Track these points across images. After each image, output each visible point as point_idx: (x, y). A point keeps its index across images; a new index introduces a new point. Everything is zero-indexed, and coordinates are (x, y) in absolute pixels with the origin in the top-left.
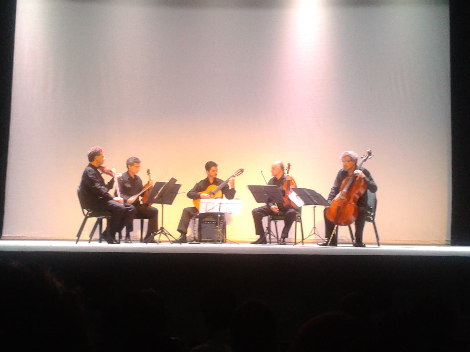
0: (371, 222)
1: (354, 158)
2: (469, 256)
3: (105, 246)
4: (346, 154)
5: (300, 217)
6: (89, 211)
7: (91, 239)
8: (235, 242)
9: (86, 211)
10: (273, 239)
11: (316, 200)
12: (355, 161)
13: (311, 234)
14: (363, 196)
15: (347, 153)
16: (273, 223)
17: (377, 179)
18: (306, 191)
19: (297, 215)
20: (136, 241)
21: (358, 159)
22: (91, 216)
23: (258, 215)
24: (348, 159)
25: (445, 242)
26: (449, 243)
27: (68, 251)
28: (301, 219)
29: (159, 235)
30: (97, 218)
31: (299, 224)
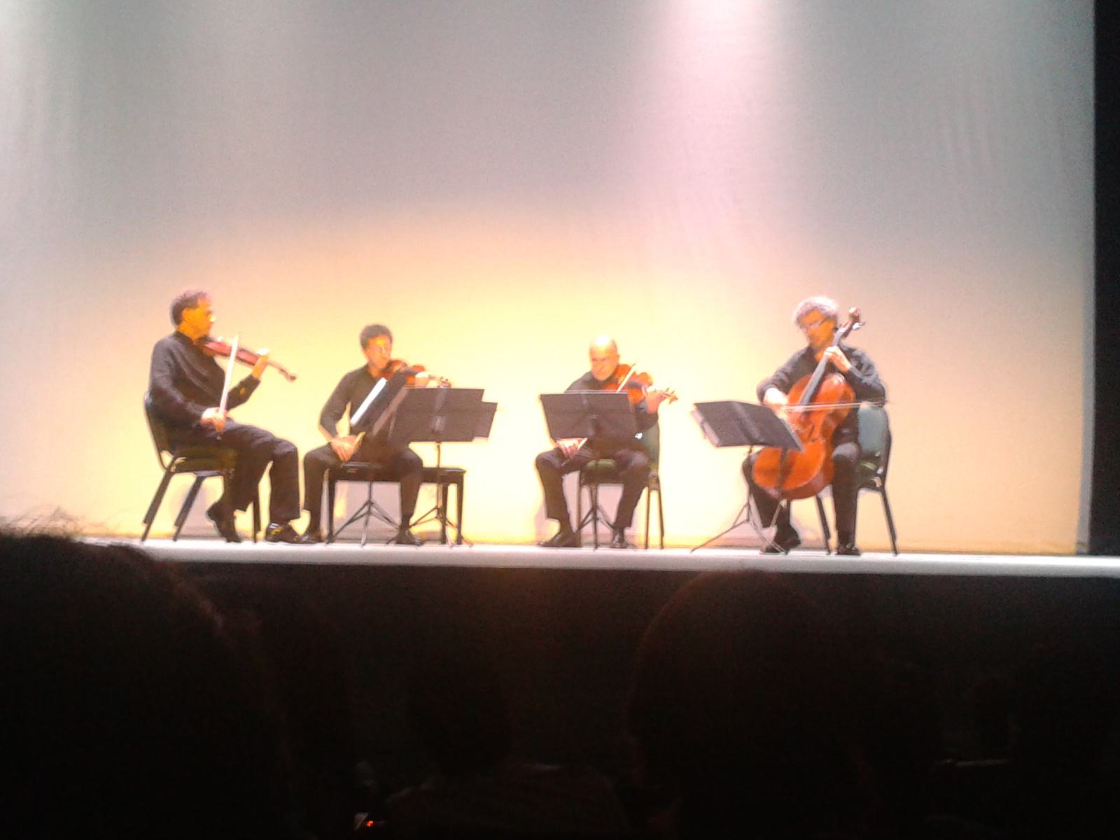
2: (1116, 576)
7: (179, 530)
9: (167, 458)
12: (831, 319)
13: (737, 523)
17: (886, 373)
18: (739, 409)
21: (839, 316)
22: (181, 469)
25: (1073, 548)
26: (1085, 550)
27: (633, 567)
28: (658, 481)
31: (654, 495)
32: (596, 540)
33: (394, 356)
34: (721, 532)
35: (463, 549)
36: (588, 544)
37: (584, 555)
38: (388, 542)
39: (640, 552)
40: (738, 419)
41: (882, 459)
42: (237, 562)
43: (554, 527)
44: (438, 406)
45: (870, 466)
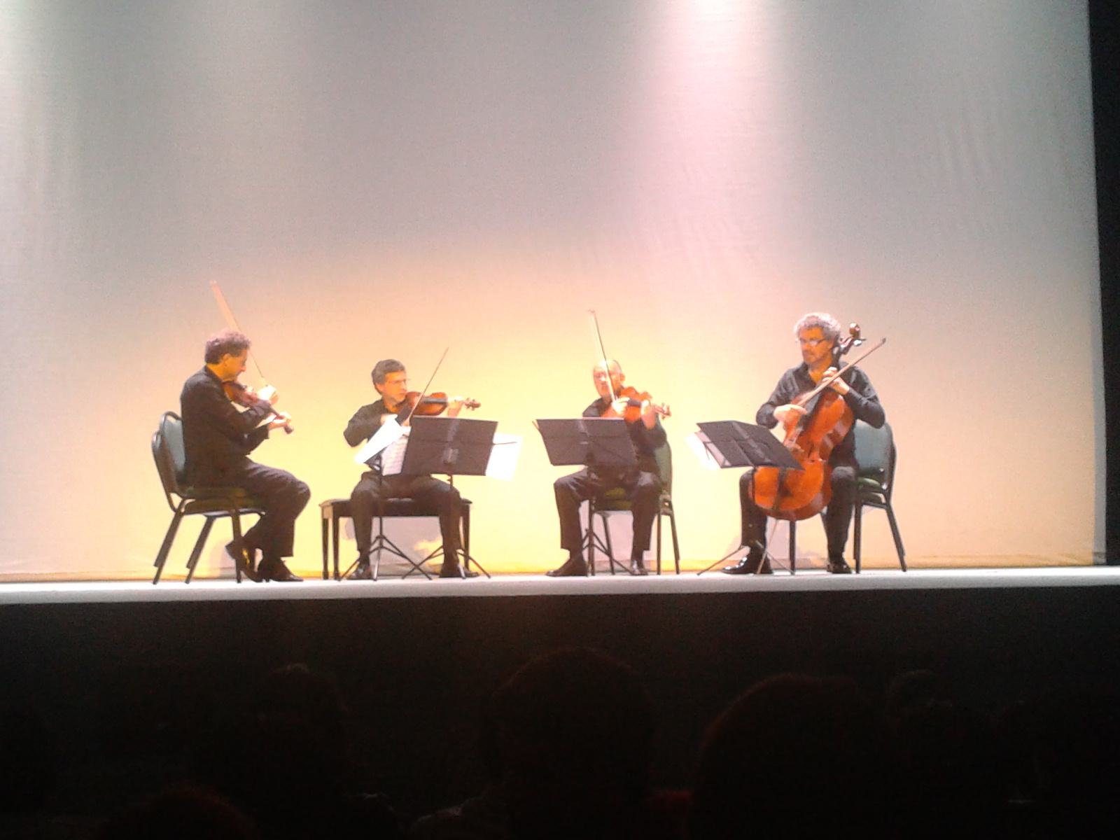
0: (881, 507)
1: (832, 332)
3: (249, 587)
4: (814, 321)
6: (184, 499)
7: (191, 572)
8: (509, 574)
9: (177, 499)
14: (844, 441)
15: (813, 317)
16: (597, 518)
18: (738, 428)
22: (191, 510)
23: (567, 497)
24: (816, 333)
25: (1091, 559)
26: (1104, 560)
28: (670, 506)
29: (376, 553)
30: (206, 516)
32: (414, 565)
33: (410, 388)
34: (725, 557)
35: (864, 574)
37: (599, 581)
39: (652, 577)
40: (809, 443)
41: (885, 474)
43: (564, 556)
44: (450, 438)
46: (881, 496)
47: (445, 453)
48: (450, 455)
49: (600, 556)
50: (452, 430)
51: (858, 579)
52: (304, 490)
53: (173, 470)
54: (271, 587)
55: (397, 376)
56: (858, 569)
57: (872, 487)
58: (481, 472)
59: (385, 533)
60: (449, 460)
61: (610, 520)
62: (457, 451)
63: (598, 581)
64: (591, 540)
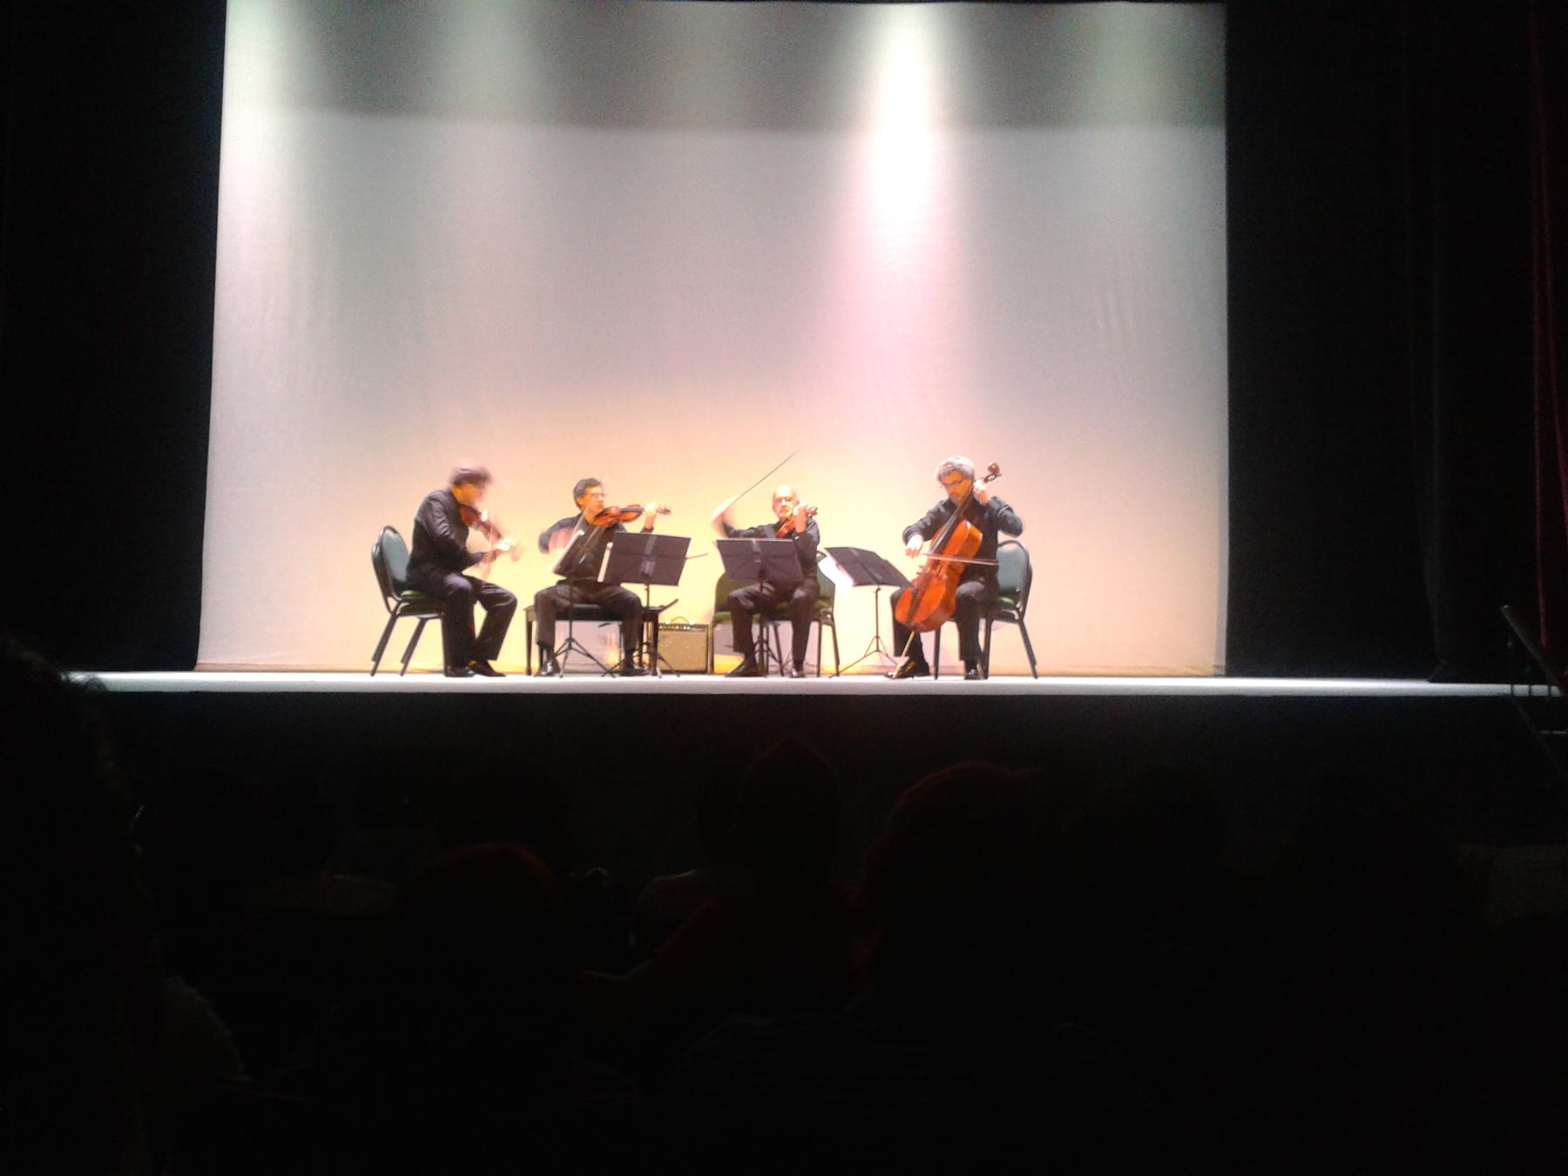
5: (832, 615)
10: (773, 666)
11: (881, 574)
19: (822, 611)
20: (811, 673)
22: (406, 612)
25: (1212, 671)
26: (1223, 673)
28: (832, 619)
36: (775, 673)
38: (611, 672)
39: (811, 680)
41: (1021, 594)
42: (1395, 695)
45: (1006, 600)
46: (1015, 612)
47: (643, 565)
48: (648, 567)
49: (772, 662)
50: (650, 543)
51: (936, 684)
52: (511, 601)
53: (390, 579)
54: (476, 682)
55: (595, 490)
56: (936, 675)
57: (1008, 606)
58: (675, 583)
59: (574, 636)
60: (646, 571)
61: (780, 629)
62: (653, 564)
63: (773, 683)
64: (762, 646)
